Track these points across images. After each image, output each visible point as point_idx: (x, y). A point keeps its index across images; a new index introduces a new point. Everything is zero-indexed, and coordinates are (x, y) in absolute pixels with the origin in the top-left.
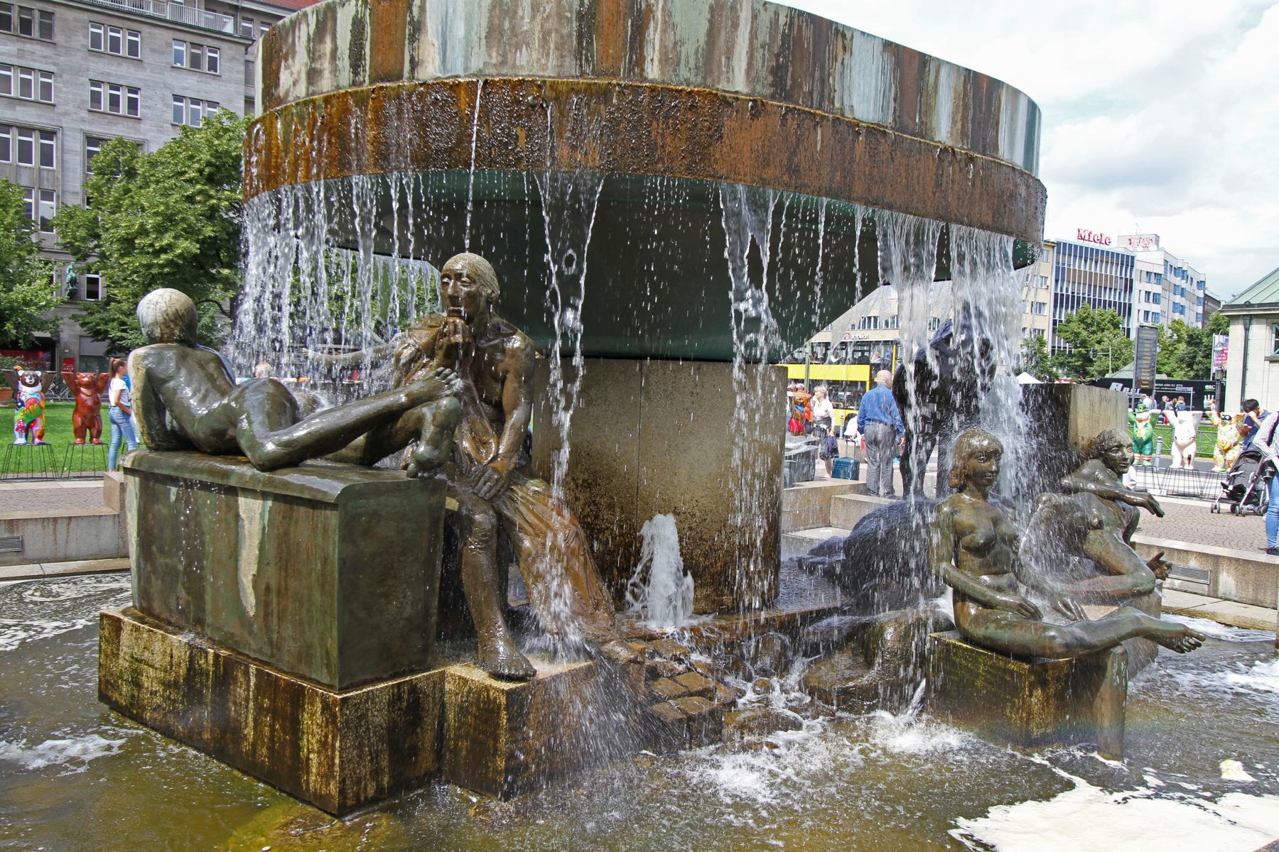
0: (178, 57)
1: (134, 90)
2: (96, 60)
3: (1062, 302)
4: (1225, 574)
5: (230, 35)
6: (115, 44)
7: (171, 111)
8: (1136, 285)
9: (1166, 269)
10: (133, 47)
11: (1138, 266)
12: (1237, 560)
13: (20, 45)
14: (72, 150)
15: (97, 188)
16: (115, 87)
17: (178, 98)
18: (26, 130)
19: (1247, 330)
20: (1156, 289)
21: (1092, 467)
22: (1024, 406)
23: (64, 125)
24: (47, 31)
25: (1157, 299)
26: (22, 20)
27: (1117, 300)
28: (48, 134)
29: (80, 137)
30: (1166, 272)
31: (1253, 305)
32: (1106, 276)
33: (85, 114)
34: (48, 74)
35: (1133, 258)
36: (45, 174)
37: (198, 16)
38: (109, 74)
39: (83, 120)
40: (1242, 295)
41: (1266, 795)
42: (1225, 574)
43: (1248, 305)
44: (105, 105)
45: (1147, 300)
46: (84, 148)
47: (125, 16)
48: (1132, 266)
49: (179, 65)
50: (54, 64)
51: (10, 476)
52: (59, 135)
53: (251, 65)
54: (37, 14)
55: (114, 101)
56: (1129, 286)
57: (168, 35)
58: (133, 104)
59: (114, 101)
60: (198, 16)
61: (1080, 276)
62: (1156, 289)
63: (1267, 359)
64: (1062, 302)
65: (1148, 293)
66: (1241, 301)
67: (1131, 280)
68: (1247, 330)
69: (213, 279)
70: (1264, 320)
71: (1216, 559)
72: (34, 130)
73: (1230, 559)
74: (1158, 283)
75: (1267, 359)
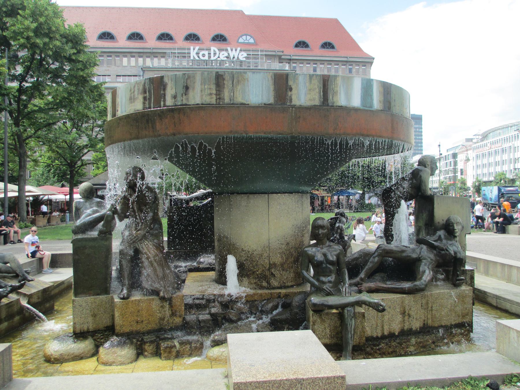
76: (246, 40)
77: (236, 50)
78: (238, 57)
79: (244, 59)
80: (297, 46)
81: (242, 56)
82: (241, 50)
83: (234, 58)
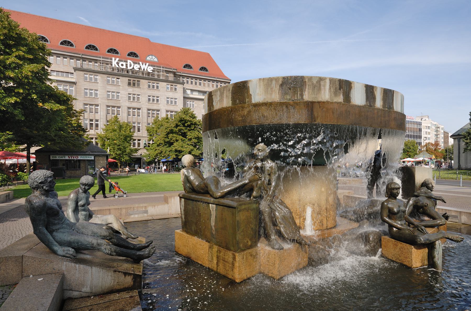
0: (168, 88)
1: (158, 97)
2: (149, 91)
3: (416, 137)
4: (463, 216)
6: (153, 86)
7: (166, 101)
8: (423, 130)
9: (431, 125)
10: (157, 87)
11: (423, 124)
12: (467, 213)
13: (133, 89)
14: (144, 112)
15: (285, 78)
16: (154, 97)
17: (168, 98)
18: (134, 108)
23: (142, 107)
24: (139, 85)
26: (133, 83)
27: (409, 134)
28: (139, 109)
29: (146, 109)
32: (413, 128)
33: (147, 104)
34: (139, 95)
35: (421, 122)
36: (138, 119)
38: (152, 94)
39: (147, 105)
42: (463, 216)
44: (151, 101)
47: (156, 80)
48: (421, 125)
49: (168, 90)
50: (140, 93)
52: (141, 109)
53: (108, 212)
54: (136, 81)
55: (153, 100)
56: (420, 130)
57: (165, 84)
58: (158, 100)
59: (153, 100)
61: (418, 130)
64: (416, 137)
65: (426, 132)
66: (457, 134)
67: (421, 129)
71: (460, 212)
73: (464, 212)
76: (152, 59)
77: (146, 65)
78: (147, 70)
79: (151, 71)
81: (150, 69)
82: (149, 65)
83: (144, 69)
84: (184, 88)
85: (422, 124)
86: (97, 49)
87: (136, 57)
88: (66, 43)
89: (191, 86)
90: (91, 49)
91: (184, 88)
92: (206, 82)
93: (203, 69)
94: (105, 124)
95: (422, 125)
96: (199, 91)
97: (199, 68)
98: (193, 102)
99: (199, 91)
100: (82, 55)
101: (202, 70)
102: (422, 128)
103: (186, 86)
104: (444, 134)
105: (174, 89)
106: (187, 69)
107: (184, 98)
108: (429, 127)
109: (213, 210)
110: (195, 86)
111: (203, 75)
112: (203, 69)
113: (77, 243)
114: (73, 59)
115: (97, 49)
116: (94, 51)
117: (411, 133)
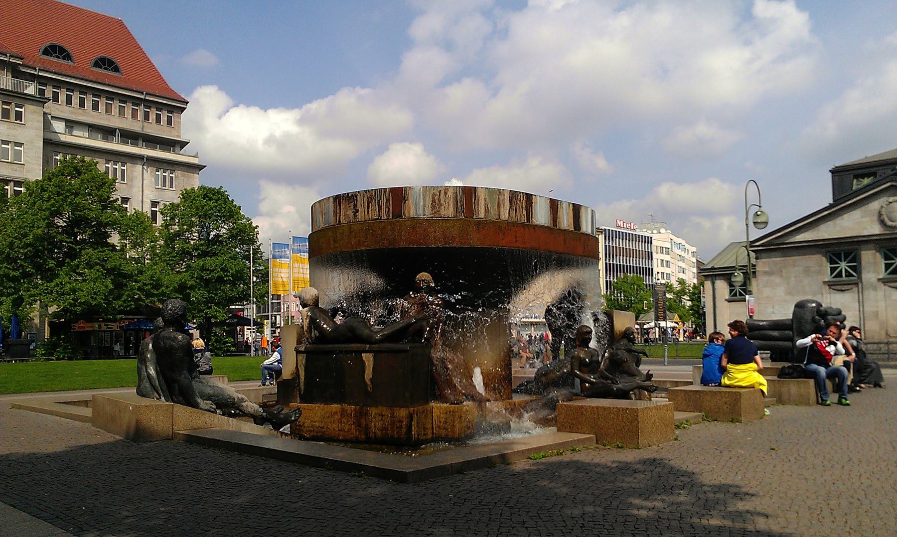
5: (32, 96)
9: (672, 244)
19: (713, 283)
20: (667, 258)
21: (624, 342)
22: (627, 328)
25: (668, 264)
30: (672, 247)
31: (716, 269)
35: (651, 238)
37: (745, 536)
40: (710, 262)
41: (256, 217)
43: (713, 268)
45: (662, 265)
46: (860, 263)
48: (651, 243)
51: (167, 87)
56: (650, 256)
60: (745, 536)
62: (667, 258)
63: (726, 300)
67: (652, 252)
68: (713, 283)
69: (418, 438)
70: (722, 277)
72: (10, 181)
74: (668, 253)
75: (726, 300)
80: (46, 52)
84: (45, 113)
85: (653, 241)
86: (116, 70)
87: (64, 58)
88: (105, 65)
89: (67, 109)
90: (105, 69)
91: (45, 113)
92: (116, 105)
93: (104, 63)
94: (727, 298)
95: (653, 245)
96: (93, 128)
97: (93, 61)
98: (123, 164)
99: (93, 128)
100: (39, 70)
101: (100, 67)
102: (653, 251)
103: (51, 108)
104: (698, 268)
105: (13, 115)
106: (55, 60)
107: (47, 143)
108: (668, 251)
109: (369, 361)
110: (81, 111)
111: (107, 81)
112: (104, 63)
113: (218, 396)
114: (73, 90)
115: (116, 70)
116: (62, 61)
117: (611, 261)
